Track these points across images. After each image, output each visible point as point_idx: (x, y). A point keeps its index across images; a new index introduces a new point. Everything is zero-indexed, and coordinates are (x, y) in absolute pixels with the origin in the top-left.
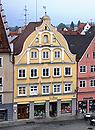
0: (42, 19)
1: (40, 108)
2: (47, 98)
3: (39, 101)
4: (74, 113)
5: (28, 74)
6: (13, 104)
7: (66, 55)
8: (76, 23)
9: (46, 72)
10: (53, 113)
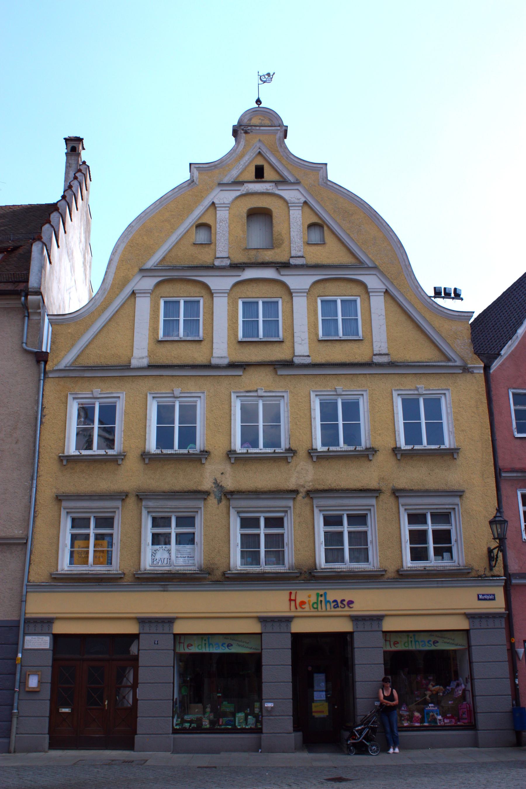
2: (275, 602)
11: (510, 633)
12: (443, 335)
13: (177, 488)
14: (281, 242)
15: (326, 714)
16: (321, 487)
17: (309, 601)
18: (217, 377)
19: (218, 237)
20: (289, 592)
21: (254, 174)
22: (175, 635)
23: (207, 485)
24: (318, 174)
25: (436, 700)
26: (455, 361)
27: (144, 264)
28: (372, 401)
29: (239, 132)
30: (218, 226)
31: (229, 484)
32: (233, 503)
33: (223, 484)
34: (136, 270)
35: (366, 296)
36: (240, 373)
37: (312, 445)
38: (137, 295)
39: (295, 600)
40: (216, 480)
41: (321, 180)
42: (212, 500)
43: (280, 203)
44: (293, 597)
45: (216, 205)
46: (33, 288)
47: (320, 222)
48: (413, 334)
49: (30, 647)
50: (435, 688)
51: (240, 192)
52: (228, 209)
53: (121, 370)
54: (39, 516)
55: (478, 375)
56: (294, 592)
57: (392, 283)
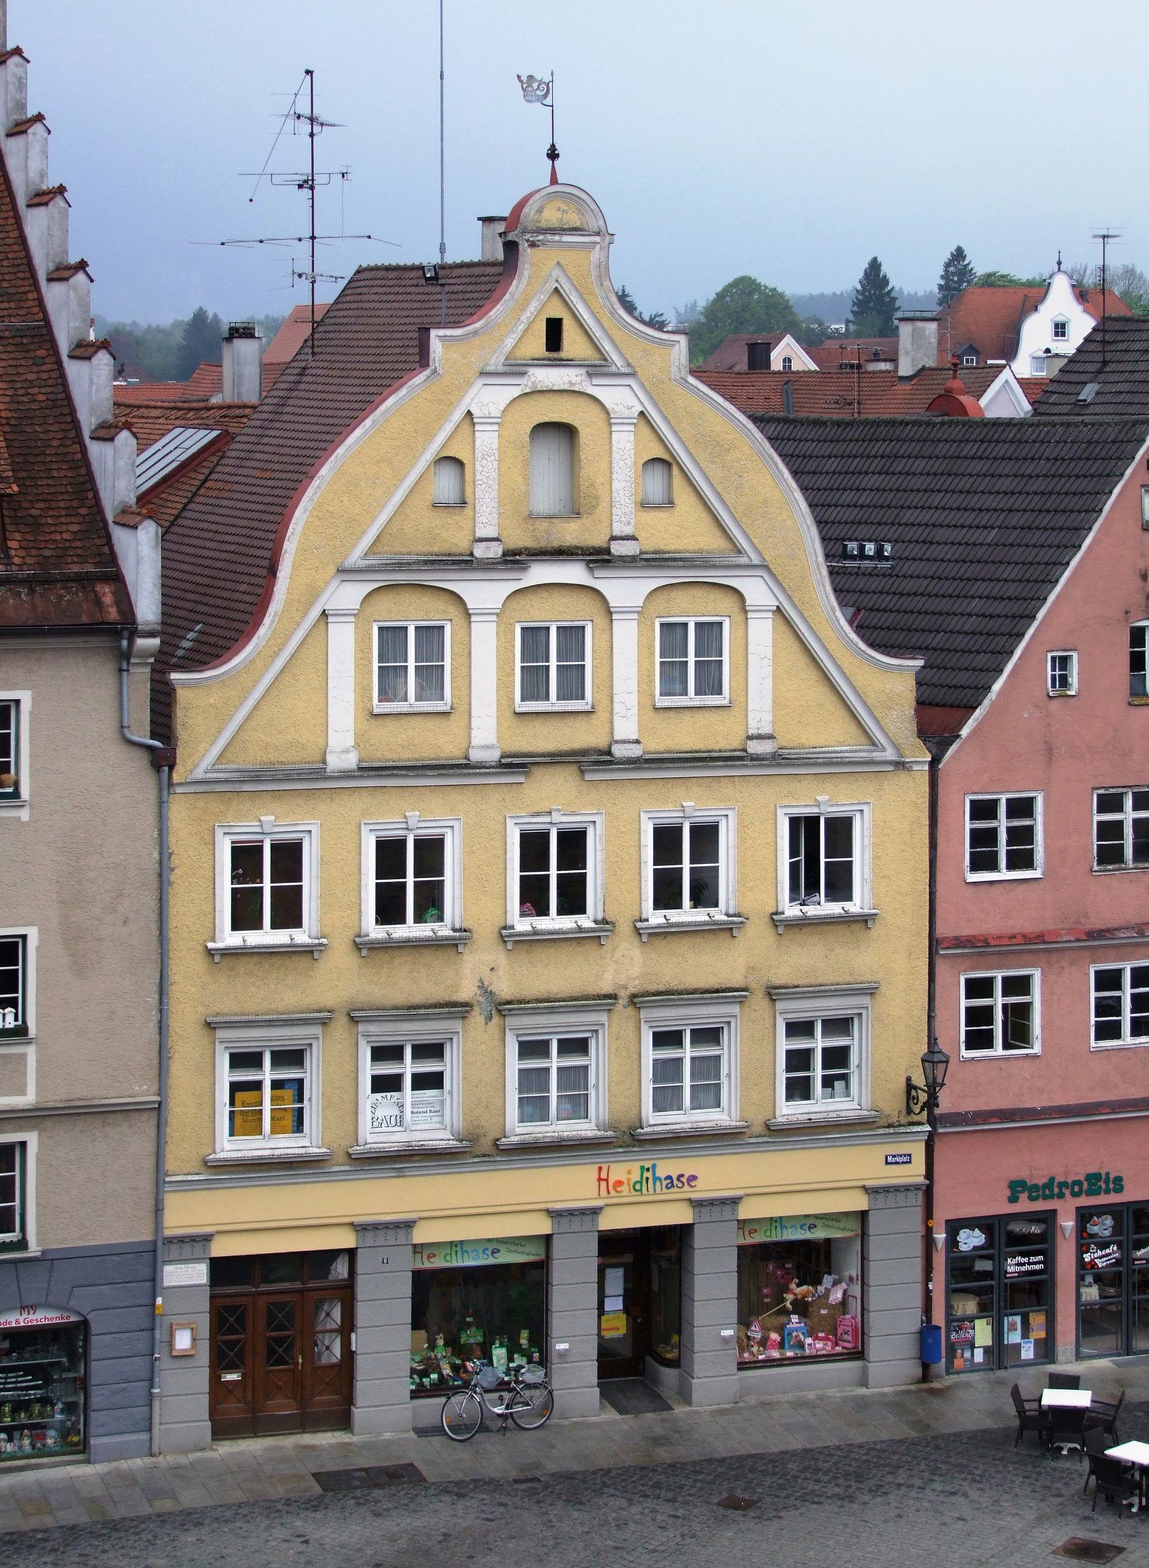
0: (512, 238)
1: (482, 1305)
2: (574, 1184)
3: (480, 1214)
4: (891, 1362)
5: (339, 888)
6: (152, 1254)
7: (795, 666)
8: (916, 279)
9: (554, 868)
10: (640, 1359)
11: (928, 1214)
12: (869, 702)
13: (417, 999)
14: (594, 503)
15: (623, 1331)
16: (653, 988)
17: (629, 1180)
18: (480, 788)
19: (479, 493)
20: (597, 1166)
21: (543, 340)
22: (415, 1246)
23: (467, 991)
24: (669, 354)
25: (802, 1308)
26: (884, 750)
27: (346, 557)
28: (742, 826)
29: (521, 248)
30: (478, 468)
31: (504, 988)
32: (511, 1021)
33: (494, 988)
34: (332, 570)
35: (741, 617)
36: (521, 779)
37: (641, 913)
38: (330, 619)
39: (607, 1180)
40: (481, 981)
41: (674, 369)
42: (477, 1017)
43: (595, 410)
44: (604, 1175)
45: (475, 420)
46: (147, 623)
47: (666, 457)
48: (817, 692)
49: (173, 1284)
50: (798, 1290)
51: (519, 388)
52: (496, 427)
53: (309, 777)
54: (176, 1056)
55: (919, 774)
56: (605, 1167)
57: (790, 598)
